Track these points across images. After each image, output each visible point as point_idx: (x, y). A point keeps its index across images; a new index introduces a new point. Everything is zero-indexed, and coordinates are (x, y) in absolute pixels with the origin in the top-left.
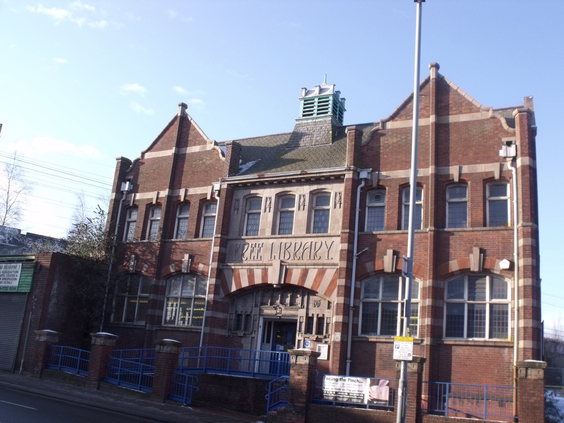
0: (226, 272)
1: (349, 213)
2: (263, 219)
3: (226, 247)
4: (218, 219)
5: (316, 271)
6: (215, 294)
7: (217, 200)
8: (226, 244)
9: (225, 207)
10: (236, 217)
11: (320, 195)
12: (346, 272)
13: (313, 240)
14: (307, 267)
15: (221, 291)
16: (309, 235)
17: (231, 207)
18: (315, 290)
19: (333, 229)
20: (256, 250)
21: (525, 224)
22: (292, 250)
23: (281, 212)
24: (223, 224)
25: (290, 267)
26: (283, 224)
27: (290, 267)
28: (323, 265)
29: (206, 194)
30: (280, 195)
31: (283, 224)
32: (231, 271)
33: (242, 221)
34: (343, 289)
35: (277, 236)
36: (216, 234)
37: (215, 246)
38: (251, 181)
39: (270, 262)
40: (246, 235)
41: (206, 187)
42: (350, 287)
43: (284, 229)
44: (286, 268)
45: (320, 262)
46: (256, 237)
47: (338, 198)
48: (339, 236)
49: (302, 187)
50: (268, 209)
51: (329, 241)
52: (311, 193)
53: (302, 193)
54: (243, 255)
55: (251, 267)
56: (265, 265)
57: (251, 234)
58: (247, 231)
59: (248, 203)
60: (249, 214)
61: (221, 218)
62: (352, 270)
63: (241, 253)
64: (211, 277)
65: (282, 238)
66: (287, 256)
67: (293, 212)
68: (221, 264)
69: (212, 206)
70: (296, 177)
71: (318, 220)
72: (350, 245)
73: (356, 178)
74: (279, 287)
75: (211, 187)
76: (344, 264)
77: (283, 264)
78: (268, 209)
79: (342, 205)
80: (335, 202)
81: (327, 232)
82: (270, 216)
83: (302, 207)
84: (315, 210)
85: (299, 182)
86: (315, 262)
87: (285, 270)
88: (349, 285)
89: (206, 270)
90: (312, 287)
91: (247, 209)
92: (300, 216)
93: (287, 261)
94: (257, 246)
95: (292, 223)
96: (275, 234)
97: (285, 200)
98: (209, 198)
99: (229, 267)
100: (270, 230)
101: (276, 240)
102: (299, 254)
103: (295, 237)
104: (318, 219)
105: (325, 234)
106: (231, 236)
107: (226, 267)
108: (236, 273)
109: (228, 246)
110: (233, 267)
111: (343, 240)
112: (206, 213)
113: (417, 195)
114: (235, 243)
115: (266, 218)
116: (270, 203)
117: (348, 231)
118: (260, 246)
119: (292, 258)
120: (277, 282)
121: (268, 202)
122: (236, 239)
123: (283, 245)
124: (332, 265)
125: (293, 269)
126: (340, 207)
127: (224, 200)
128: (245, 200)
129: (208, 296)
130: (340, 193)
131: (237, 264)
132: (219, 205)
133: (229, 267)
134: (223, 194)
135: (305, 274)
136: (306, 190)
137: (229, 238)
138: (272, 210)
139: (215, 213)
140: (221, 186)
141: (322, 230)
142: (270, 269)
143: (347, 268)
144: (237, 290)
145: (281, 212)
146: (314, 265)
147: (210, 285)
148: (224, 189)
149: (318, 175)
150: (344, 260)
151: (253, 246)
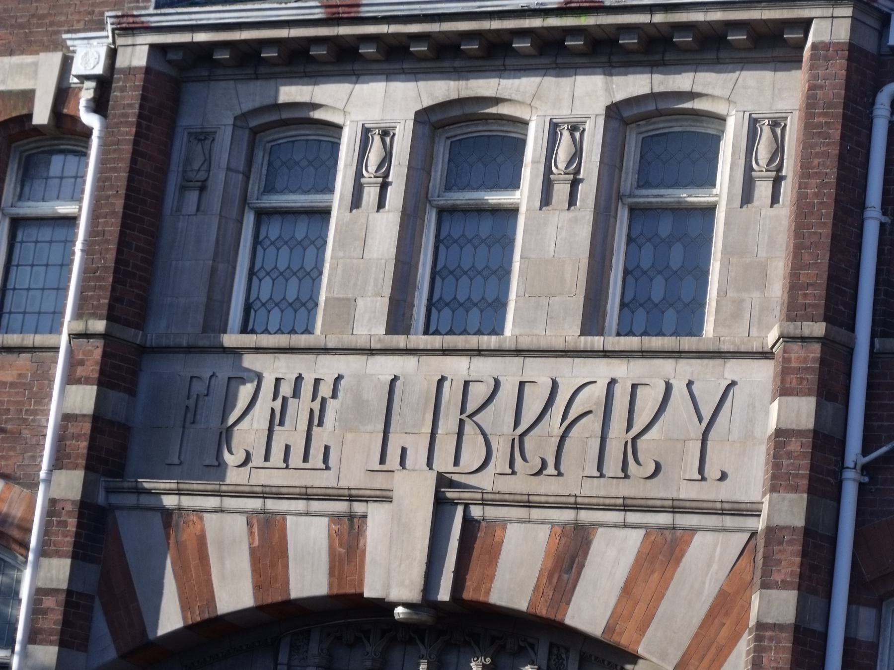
0: (131, 529)
1: (827, 231)
2: (341, 244)
3: (132, 392)
4: (92, 232)
5: (636, 537)
6: (63, 644)
7: (87, 132)
8: (135, 372)
9: (134, 172)
10: (193, 228)
11: (661, 126)
12: (804, 554)
13: (620, 369)
14: (585, 516)
15: (100, 626)
16: (597, 342)
17: (164, 170)
18: (624, 641)
19: (736, 316)
20: (299, 411)
21: (793, 329)
22: (499, 419)
23: (444, 213)
24: (119, 261)
25: (492, 512)
26: (452, 279)
27: (492, 512)
28: (676, 508)
29: (28, 96)
30: (436, 117)
31: (452, 279)
32: (157, 519)
33: (226, 253)
34: (787, 643)
35: (419, 340)
36: (79, 314)
37: (70, 379)
38: (283, 33)
39: (380, 482)
40: (244, 330)
41: (28, 59)
42: (824, 637)
43: (454, 304)
44: (468, 521)
45: (657, 490)
46: (302, 340)
47: (763, 151)
48: (766, 355)
49: (565, 82)
50: (371, 194)
51: (710, 378)
52: (614, 112)
53: (563, 112)
54: (225, 436)
55: (272, 505)
56: (351, 499)
57: (273, 325)
58: (248, 308)
59: (259, 154)
60: (262, 215)
61: (113, 228)
62: (833, 541)
63: (215, 423)
64: (44, 552)
65: (445, 352)
66: (472, 456)
67: (512, 212)
68: (103, 482)
69: (57, 162)
70: (536, 23)
71: (646, 264)
72: (830, 406)
73: (869, 44)
74: (424, 617)
75: (56, 59)
76: (793, 510)
77: (451, 494)
78: (371, 194)
79: (787, 189)
80: (749, 169)
81: (695, 329)
82: (383, 229)
83: (561, 191)
84: (634, 211)
85: (554, 52)
86: (625, 489)
87: (460, 526)
88: (817, 626)
89: (18, 512)
90: (609, 628)
91: (254, 187)
92: (550, 240)
93: (472, 480)
94: (307, 389)
95: (502, 273)
96: (406, 330)
97: (466, 146)
98: (41, 115)
99: (145, 500)
100: (382, 305)
101: (411, 362)
102: (541, 444)
103: (518, 352)
104: (646, 259)
105: (687, 343)
106: (159, 330)
107: (131, 500)
108: (187, 536)
109: (144, 382)
110: (169, 501)
111: (792, 381)
112: (20, 197)
113: (749, 155)
114: (180, 368)
115: (362, 242)
116: (387, 158)
117: (819, 329)
118: (325, 390)
119: (499, 462)
120: (413, 594)
121: (374, 156)
122: (191, 349)
123: (451, 395)
124: (723, 513)
125: (504, 523)
126: (775, 199)
127: (128, 133)
128: (245, 135)
129: (24, 655)
130: (774, 124)
131: (196, 486)
132: (102, 161)
133: (145, 500)
134: (127, 98)
135: (570, 556)
136: (588, 95)
137: (152, 339)
138: (395, 196)
139: (77, 198)
140: (112, 54)
141: (670, 317)
142: (377, 518)
143: (809, 531)
144: (187, 628)
145: (444, 213)
146: (625, 508)
147: (39, 593)
148: (130, 71)
149: (659, 18)
150: (795, 489)
151: (286, 389)
